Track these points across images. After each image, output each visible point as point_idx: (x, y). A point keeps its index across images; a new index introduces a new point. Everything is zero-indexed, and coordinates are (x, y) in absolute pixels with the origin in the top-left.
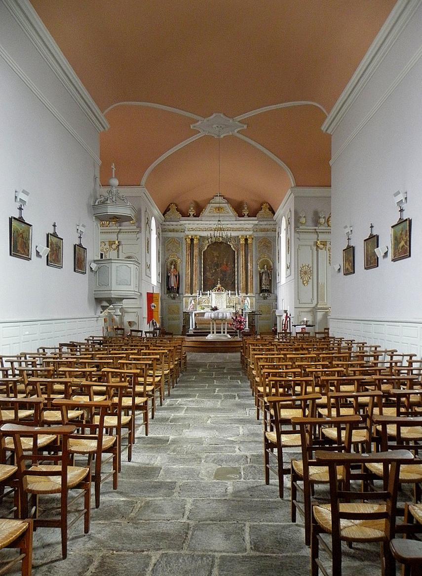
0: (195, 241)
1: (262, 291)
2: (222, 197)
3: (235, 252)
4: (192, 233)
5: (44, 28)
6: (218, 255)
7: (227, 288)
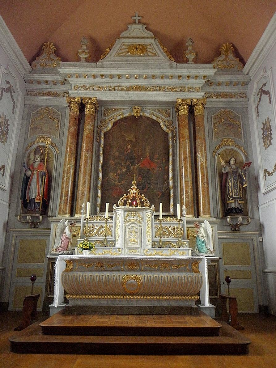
0: (89, 109)
1: (227, 212)
2: (145, 26)
3: (167, 134)
4: (84, 94)
5: (104, 325)
6: (134, 140)
7: (153, 201)
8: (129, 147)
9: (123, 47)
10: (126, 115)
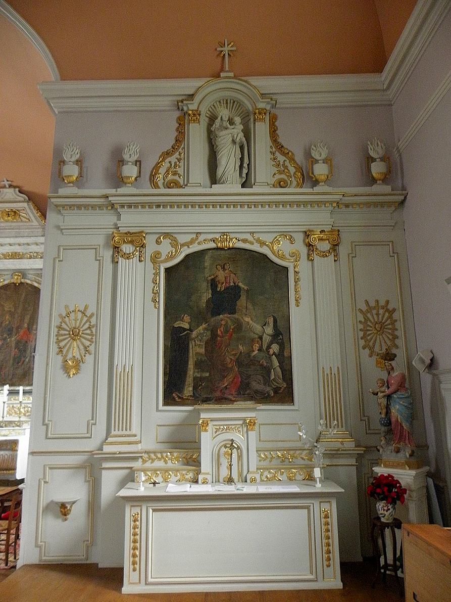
2: (17, 189)
6: (13, 310)
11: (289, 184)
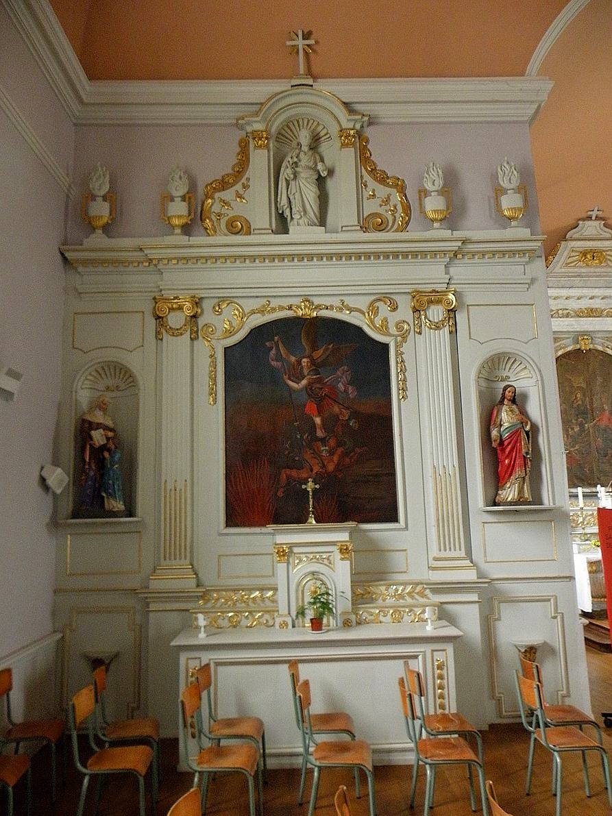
8: (579, 396)
9: (574, 254)
10: (570, 349)
11: (390, 224)
